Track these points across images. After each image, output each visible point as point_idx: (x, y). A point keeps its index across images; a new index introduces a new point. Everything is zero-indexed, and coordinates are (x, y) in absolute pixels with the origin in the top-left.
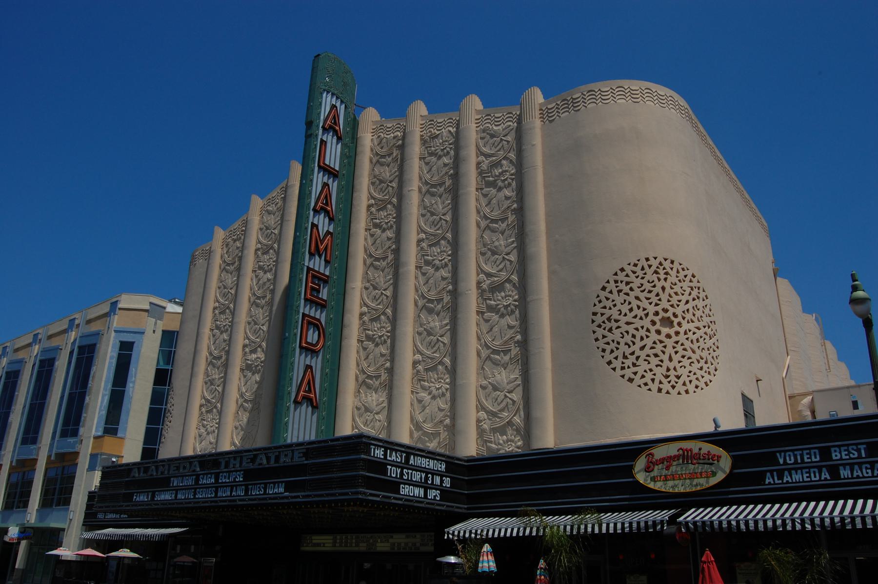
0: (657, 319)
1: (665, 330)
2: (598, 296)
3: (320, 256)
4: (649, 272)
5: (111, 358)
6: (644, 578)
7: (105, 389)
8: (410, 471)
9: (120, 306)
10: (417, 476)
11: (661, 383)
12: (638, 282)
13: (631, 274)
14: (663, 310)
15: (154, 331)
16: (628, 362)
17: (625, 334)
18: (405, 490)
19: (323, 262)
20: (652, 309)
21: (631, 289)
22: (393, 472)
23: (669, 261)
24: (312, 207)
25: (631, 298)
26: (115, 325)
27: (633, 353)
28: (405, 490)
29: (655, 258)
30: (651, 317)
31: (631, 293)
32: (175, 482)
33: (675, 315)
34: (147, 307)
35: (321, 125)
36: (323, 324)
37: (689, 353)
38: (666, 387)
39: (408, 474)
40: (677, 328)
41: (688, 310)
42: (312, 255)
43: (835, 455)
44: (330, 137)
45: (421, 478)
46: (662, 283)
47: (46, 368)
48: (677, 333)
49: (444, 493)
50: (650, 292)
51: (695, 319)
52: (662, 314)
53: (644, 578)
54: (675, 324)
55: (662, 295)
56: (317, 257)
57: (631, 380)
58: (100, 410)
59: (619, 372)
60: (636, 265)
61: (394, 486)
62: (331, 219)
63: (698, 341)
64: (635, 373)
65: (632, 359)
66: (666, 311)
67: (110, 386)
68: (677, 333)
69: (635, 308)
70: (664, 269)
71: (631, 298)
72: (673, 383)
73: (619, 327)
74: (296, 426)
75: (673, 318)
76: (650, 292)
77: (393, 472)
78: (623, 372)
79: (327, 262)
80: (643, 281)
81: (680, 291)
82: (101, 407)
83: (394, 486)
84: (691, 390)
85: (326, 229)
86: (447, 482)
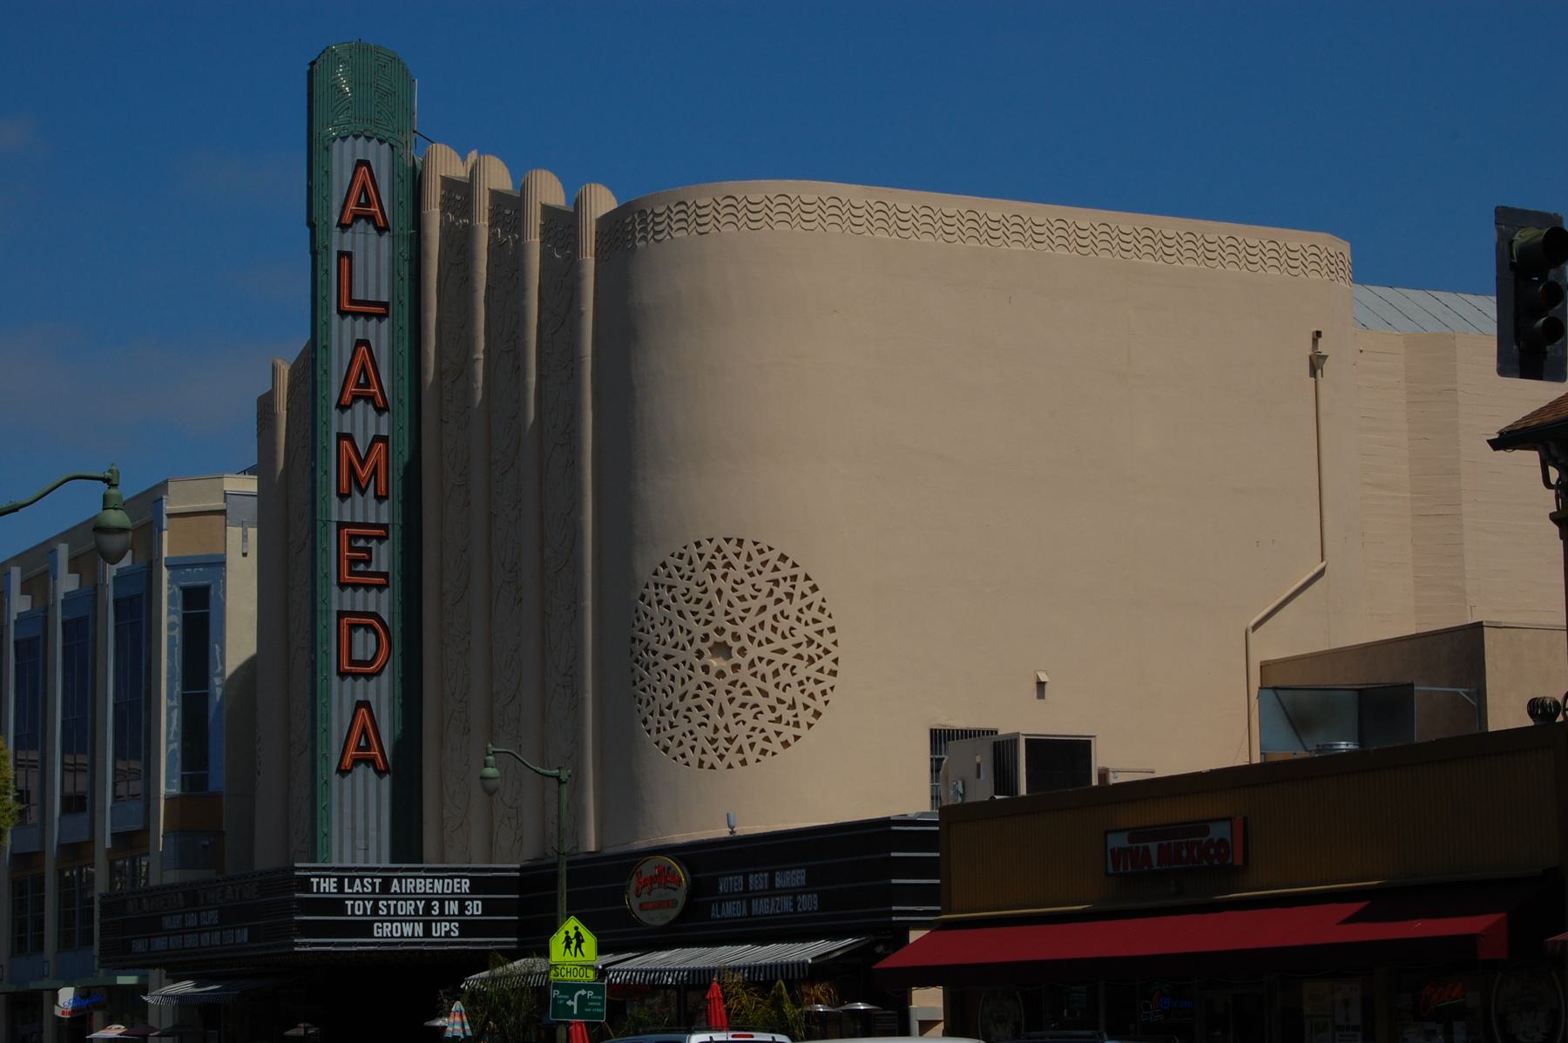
1: (716, 663)
2: (770, 549)
3: (363, 492)
5: (171, 626)
7: (170, 696)
8: (392, 903)
9: (168, 507)
10: (409, 907)
14: (717, 630)
15: (245, 555)
17: (787, 633)
18: (382, 931)
19: (372, 502)
20: (699, 630)
21: (773, 709)
22: (357, 909)
24: (334, 403)
25: (763, 599)
26: (165, 554)
28: (382, 931)
29: (710, 540)
30: (729, 628)
32: (166, 922)
33: (736, 637)
34: (218, 504)
35: (336, 218)
36: (385, 618)
37: (712, 710)
38: (711, 757)
39: (388, 907)
40: (736, 658)
42: (342, 496)
43: (419, 929)
44: (360, 238)
45: (416, 909)
47: (80, 631)
48: (736, 667)
49: (468, 927)
52: (714, 637)
56: (357, 495)
58: (169, 742)
61: (364, 928)
62: (379, 411)
66: (720, 631)
67: (178, 688)
68: (736, 667)
70: (724, 557)
74: (347, 810)
75: (730, 642)
77: (357, 909)
79: (380, 499)
82: (168, 734)
83: (364, 928)
84: (751, 760)
85: (372, 433)
86: (475, 908)
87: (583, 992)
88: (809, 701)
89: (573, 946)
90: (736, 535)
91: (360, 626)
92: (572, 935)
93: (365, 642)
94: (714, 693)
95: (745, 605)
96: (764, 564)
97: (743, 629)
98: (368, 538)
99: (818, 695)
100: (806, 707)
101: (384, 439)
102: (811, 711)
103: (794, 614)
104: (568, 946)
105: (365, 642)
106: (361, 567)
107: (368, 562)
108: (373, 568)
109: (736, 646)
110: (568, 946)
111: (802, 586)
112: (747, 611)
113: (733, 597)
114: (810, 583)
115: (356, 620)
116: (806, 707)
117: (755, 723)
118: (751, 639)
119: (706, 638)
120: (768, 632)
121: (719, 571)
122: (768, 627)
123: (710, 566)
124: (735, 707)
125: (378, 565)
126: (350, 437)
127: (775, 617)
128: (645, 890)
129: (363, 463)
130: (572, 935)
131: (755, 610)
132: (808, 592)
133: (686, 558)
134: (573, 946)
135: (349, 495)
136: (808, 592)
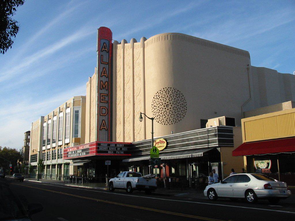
0: (167, 108)
3: (104, 89)
4: (181, 114)
6: (287, 105)
11: (178, 119)
12: (180, 99)
13: (155, 116)
16: (157, 97)
19: (105, 90)
21: (159, 115)
23: (152, 106)
25: (177, 113)
27: (177, 98)
30: (166, 110)
31: (160, 115)
41: (163, 100)
46: (157, 107)
50: (160, 110)
51: (165, 97)
52: (165, 107)
53: (287, 105)
54: (168, 104)
55: (160, 107)
56: (103, 89)
57: (184, 116)
59: (156, 95)
60: (154, 114)
63: (171, 97)
64: (155, 99)
65: (158, 98)
66: (168, 109)
69: (164, 114)
71: (177, 113)
72: (168, 122)
73: (169, 118)
75: (166, 104)
76: (160, 110)
78: (180, 93)
80: (157, 112)
81: (158, 102)
85: (105, 81)
87: (156, 160)
88: (160, 121)
89: (155, 151)
90: (183, 94)
91: (104, 108)
92: (154, 149)
93: (104, 111)
94: (161, 105)
95: (164, 114)
96: (183, 101)
97: (164, 110)
98: (105, 96)
99: (161, 122)
100: (159, 120)
101: (107, 82)
102: (159, 121)
103: (162, 95)
104: (154, 151)
105: (104, 111)
106: (103, 100)
107: (105, 99)
108: (105, 100)
109: (167, 104)
110: (154, 151)
111: (180, 119)
112: (164, 113)
113: (166, 115)
114: (180, 120)
115: (109, 110)
116: (159, 120)
117: (157, 112)
118: (165, 101)
119: (168, 109)
120: (160, 110)
121: (168, 119)
122: (160, 111)
123: (159, 118)
124: (159, 109)
125: (106, 100)
126: (102, 81)
127: (174, 114)
128: (157, 144)
129: (104, 85)
130: (154, 149)
131: (177, 105)
132: (158, 93)
133: (161, 122)
134: (155, 151)
135: (102, 89)
136: (158, 93)
